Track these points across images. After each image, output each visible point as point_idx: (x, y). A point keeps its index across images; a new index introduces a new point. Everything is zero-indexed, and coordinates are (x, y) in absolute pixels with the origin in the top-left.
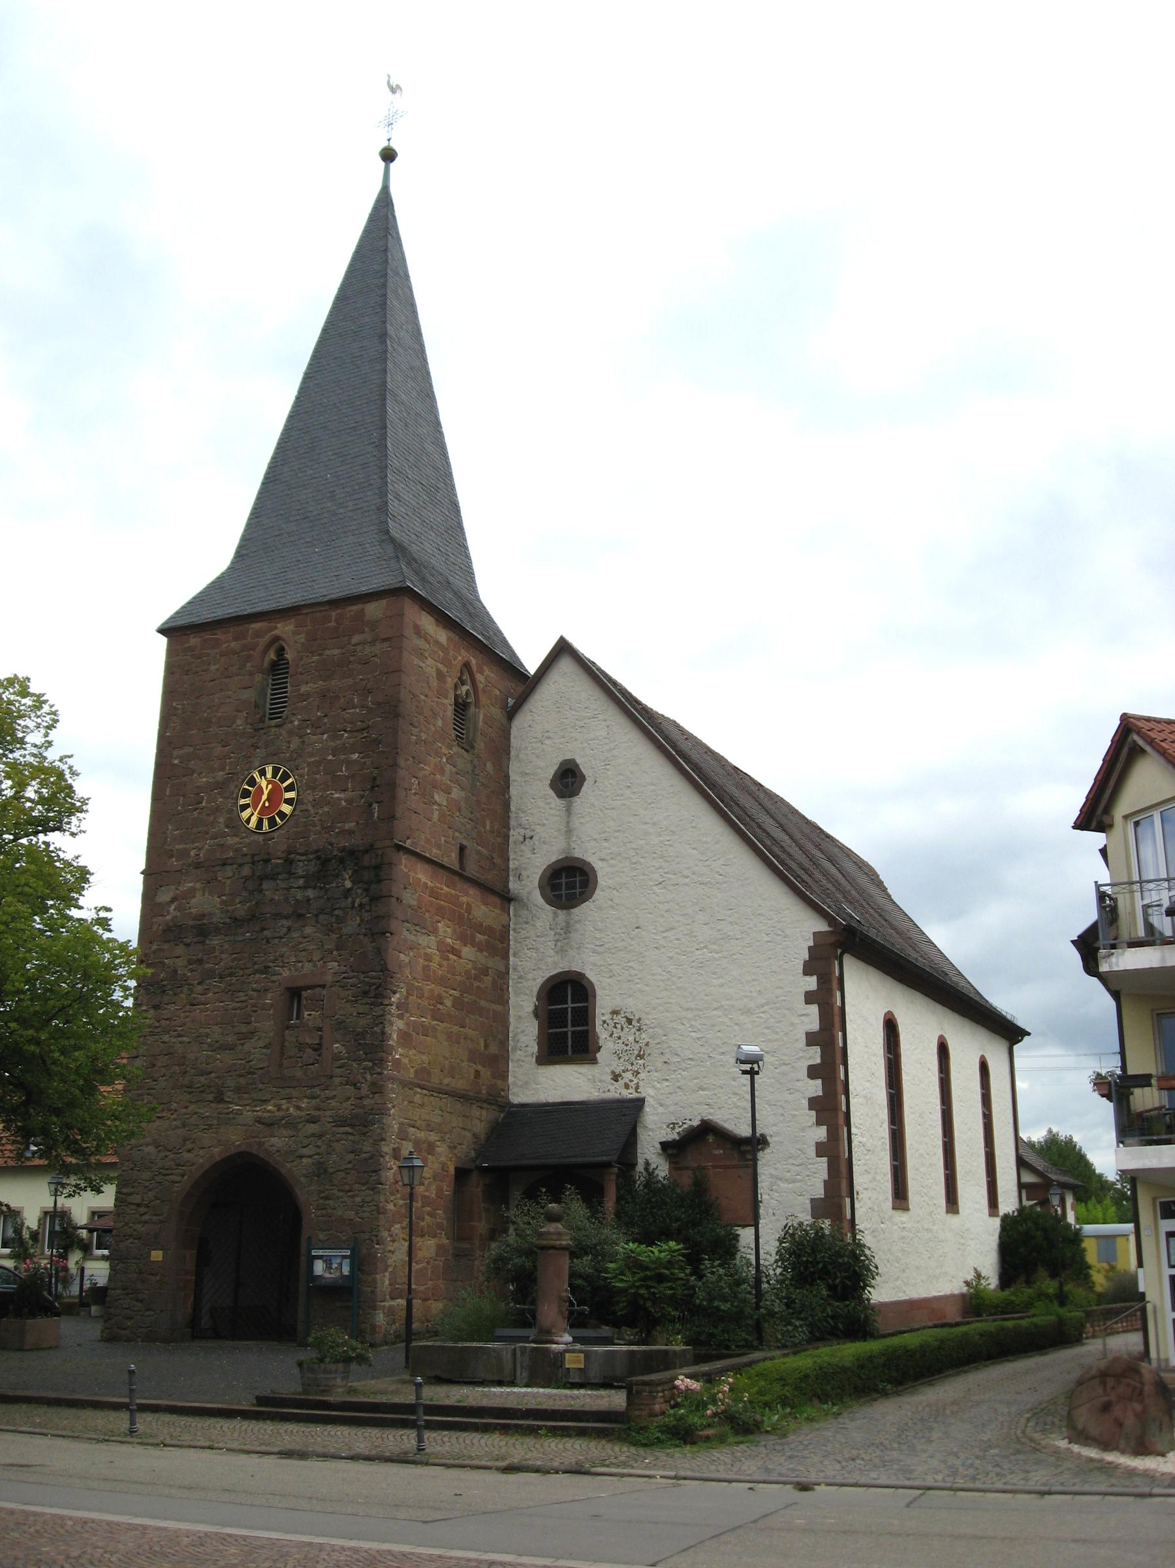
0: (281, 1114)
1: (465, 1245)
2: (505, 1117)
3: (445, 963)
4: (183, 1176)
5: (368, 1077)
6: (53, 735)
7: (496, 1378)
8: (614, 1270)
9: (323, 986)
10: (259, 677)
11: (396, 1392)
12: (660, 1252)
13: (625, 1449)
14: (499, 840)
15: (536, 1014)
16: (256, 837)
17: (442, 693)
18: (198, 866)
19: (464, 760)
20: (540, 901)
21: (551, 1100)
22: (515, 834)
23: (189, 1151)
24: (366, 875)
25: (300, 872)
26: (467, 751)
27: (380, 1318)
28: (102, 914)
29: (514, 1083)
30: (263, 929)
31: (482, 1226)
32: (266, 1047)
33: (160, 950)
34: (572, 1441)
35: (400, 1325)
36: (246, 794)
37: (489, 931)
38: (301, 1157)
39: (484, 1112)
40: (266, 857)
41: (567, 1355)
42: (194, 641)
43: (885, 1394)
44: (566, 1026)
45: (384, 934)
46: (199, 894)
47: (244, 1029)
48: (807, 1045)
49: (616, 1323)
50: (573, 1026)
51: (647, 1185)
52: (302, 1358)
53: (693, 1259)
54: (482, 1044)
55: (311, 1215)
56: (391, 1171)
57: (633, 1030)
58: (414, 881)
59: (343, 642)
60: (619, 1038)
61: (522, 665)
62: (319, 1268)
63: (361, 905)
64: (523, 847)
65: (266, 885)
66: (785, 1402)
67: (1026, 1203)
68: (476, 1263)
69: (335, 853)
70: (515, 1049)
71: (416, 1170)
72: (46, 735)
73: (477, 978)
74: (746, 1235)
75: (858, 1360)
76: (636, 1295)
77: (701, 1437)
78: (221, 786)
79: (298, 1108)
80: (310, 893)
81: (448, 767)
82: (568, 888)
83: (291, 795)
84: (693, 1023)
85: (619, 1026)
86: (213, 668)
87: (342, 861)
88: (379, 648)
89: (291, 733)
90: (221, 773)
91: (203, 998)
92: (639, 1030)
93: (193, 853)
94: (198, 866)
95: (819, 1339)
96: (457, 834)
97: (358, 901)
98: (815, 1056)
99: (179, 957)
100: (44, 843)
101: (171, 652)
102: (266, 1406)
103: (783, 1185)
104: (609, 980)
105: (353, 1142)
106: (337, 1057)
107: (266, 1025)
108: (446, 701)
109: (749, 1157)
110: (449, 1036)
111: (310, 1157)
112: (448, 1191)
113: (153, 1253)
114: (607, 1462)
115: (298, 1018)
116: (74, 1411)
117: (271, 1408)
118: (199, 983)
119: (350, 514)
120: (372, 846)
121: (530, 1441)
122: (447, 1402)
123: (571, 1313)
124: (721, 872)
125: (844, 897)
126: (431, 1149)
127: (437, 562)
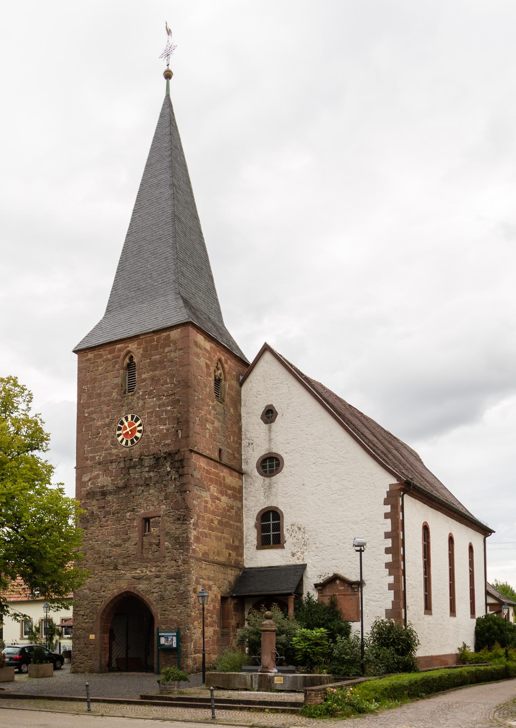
0: (143, 574)
1: (226, 630)
2: (242, 574)
3: (214, 504)
4: (102, 602)
5: (181, 557)
6: (30, 405)
7: (244, 687)
8: (296, 640)
9: (159, 517)
10: (122, 372)
11: (200, 693)
12: (316, 633)
13: (304, 719)
14: (237, 446)
15: (256, 526)
16: (125, 449)
17: (208, 375)
18: (100, 463)
19: (220, 407)
20: (257, 474)
21: (263, 565)
22: (244, 443)
23: (104, 591)
24: (177, 465)
25: (146, 464)
26: (221, 403)
27: (190, 662)
28: (61, 486)
29: (246, 558)
30: (131, 492)
31: (233, 622)
32: (135, 545)
33: (86, 503)
34: (280, 715)
35: (199, 665)
36: (119, 429)
37: (233, 489)
38: (153, 593)
39: (233, 571)
40: (130, 458)
41: (275, 678)
42: (90, 355)
43: (422, 698)
44: (270, 532)
45: (186, 491)
46: (101, 476)
47: (125, 537)
48: (385, 538)
49: (296, 663)
50: (273, 531)
51: (308, 603)
52: (159, 679)
53: (332, 636)
54: (232, 541)
55: (158, 617)
56: (193, 598)
57: (301, 533)
58: (199, 466)
59: (168, 358)
60: (295, 537)
61: (246, 359)
62: (163, 641)
63: (175, 479)
64: (248, 449)
65: (131, 471)
66: (377, 700)
67: (489, 612)
68: (231, 638)
69: (162, 454)
70: (246, 543)
71: (205, 597)
72: (28, 405)
73: (229, 511)
74: (355, 626)
75: (410, 682)
76: (306, 652)
77: (338, 714)
78: (109, 425)
79: (151, 571)
80: (152, 474)
81: (213, 412)
82: (270, 467)
83: (141, 428)
84: (329, 529)
85: (294, 531)
86: (100, 368)
87: (165, 458)
88: (178, 353)
89: (138, 398)
90: (107, 419)
91: (106, 524)
92: (304, 533)
93: (97, 458)
94: (100, 463)
95: (390, 672)
96: (218, 443)
97: (173, 477)
98: (389, 543)
99: (94, 505)
100: (31, 455)
101: (79, 362)
102: (145, 699)
103: (372, 603)
104: (290, 510)
105: (175, 585)
106: (167, 548)
107: (135, 535)
108: (210, 379)
109: (356, 590)
110: (217, 538)
111: (157, 593)
112: (218, 606)
113: (91, 636)
114: (296, 724)
115: (149, 531)
116: (63, 702)
117: (147, 700)
118: (104, 517)
119: (160, 285)
120: (179, 450)
121: (261, 714)
122: (223, 698)
123: (277, 659)
124: (344, 457)
125: (404, 467)
126: (210, 588)
127: (203, 307)
